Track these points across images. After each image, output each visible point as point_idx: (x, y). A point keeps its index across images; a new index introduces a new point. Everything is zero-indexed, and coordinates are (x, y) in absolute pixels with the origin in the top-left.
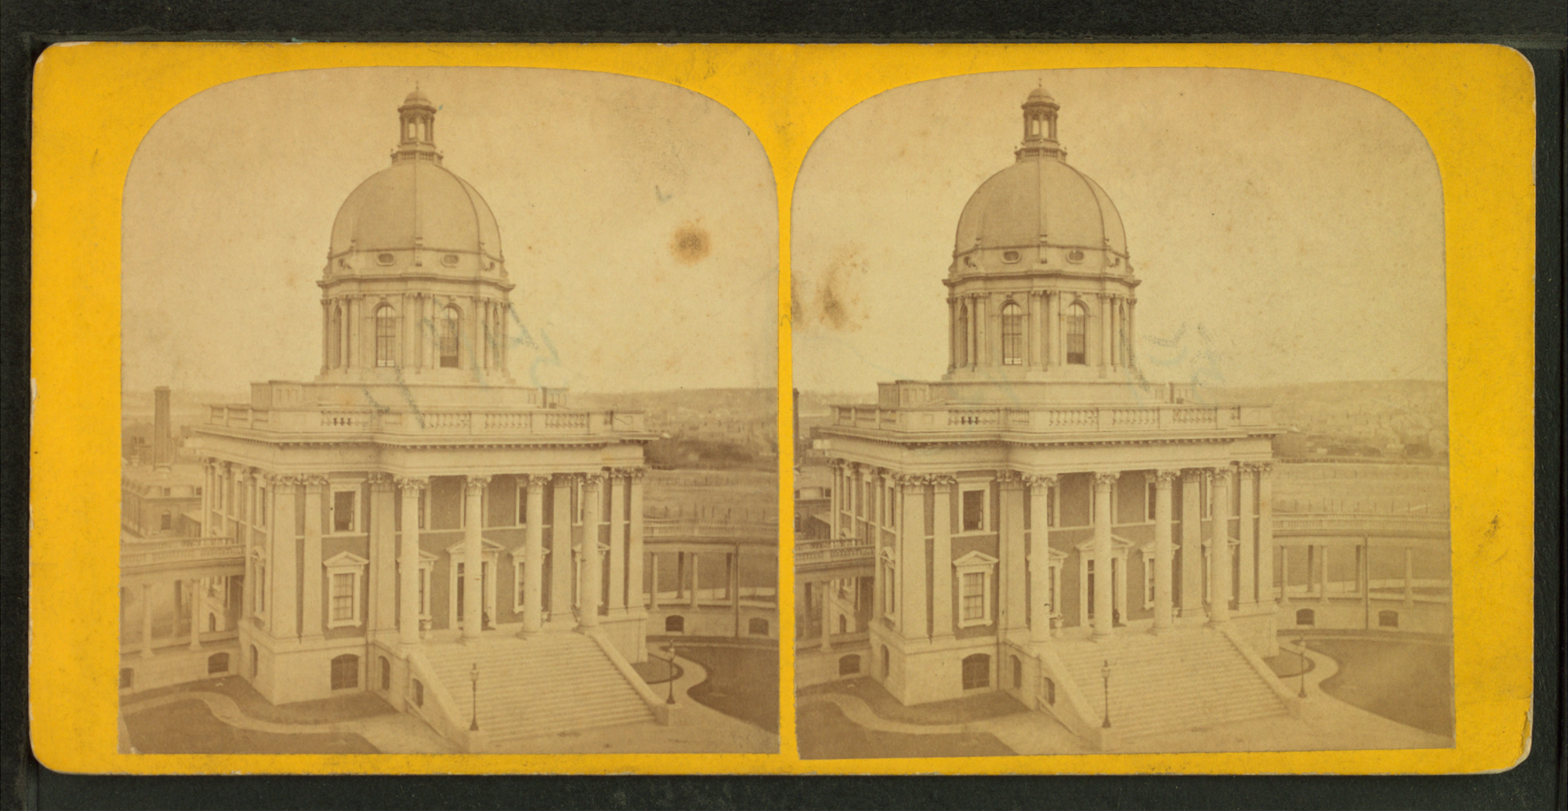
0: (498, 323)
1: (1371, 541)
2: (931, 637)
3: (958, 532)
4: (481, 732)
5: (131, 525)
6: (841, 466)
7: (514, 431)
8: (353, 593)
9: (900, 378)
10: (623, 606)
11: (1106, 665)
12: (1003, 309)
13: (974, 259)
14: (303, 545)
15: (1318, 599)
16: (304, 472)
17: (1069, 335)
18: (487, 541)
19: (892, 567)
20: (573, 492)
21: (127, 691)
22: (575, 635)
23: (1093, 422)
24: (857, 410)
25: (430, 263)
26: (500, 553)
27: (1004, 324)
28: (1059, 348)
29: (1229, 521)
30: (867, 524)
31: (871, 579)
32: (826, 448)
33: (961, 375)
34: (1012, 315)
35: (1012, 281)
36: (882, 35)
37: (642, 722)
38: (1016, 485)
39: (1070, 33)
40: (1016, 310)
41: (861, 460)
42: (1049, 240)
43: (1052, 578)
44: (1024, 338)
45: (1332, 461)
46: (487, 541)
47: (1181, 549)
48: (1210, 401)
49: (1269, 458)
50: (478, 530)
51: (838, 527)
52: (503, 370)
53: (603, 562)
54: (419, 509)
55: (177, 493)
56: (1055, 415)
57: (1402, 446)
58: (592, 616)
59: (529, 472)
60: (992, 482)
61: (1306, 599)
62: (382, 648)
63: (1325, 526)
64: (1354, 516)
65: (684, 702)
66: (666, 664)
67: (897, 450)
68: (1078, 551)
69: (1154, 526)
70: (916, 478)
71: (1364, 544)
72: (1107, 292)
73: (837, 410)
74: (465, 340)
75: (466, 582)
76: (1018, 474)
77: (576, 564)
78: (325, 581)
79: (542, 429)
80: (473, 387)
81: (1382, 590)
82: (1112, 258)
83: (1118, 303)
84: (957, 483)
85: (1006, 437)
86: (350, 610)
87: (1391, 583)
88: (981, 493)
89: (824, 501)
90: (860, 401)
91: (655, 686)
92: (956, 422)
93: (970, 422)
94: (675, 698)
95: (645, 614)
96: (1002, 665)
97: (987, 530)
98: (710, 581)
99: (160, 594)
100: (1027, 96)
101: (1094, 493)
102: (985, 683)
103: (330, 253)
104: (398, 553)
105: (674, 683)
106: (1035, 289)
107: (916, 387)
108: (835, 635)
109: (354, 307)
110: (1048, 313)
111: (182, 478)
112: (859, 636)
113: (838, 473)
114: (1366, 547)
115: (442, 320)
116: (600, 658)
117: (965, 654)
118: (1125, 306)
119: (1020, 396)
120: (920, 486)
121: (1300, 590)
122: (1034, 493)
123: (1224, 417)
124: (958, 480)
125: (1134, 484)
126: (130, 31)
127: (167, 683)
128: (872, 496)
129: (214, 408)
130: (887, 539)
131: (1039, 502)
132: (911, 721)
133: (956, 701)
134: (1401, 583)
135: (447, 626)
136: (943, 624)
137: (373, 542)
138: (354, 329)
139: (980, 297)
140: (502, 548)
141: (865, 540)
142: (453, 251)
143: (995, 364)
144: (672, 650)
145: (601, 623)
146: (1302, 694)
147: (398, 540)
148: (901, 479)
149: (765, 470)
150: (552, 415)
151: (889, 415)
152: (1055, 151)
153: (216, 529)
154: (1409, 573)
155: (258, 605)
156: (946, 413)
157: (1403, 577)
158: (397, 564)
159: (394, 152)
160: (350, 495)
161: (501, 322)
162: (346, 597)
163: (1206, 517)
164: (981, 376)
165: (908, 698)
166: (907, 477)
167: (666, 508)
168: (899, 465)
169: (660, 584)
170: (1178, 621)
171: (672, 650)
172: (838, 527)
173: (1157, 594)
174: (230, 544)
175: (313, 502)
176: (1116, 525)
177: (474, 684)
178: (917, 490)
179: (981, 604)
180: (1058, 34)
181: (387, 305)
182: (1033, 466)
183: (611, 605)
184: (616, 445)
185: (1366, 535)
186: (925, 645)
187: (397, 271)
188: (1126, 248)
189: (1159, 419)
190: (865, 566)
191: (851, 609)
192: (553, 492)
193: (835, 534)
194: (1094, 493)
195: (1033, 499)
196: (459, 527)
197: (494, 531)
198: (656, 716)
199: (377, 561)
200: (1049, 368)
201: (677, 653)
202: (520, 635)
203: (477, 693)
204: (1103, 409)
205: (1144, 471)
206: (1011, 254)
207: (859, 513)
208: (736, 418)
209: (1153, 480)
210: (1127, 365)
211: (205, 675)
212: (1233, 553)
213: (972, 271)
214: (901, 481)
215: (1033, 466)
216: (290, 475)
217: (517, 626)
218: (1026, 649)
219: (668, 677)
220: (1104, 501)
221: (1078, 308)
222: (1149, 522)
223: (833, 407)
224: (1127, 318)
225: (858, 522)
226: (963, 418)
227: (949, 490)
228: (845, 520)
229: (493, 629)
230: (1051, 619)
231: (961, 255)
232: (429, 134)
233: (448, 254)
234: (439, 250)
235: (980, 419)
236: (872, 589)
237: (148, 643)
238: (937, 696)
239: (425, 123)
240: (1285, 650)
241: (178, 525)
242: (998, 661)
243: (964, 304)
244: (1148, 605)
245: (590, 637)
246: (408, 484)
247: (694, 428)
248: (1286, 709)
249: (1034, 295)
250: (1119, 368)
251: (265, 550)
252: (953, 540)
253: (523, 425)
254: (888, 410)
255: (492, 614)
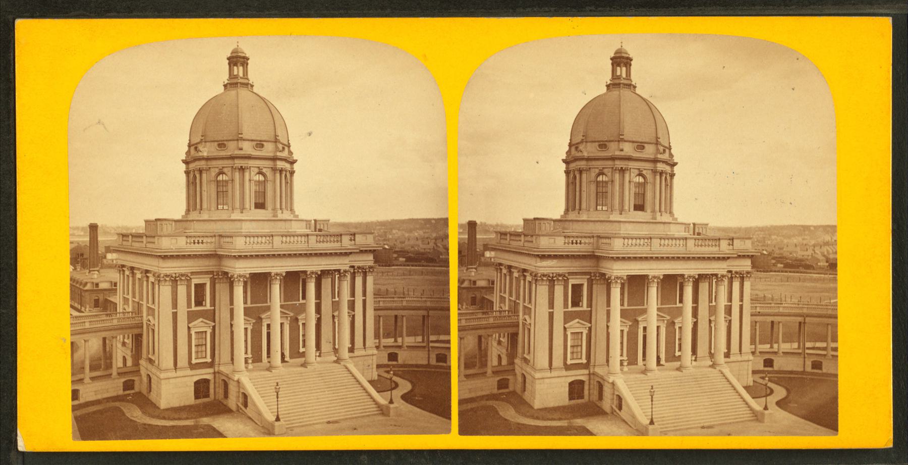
0: (287, 183)
1: (808, 319)
2: (551, 369)
3: (568, 308)
4: (282, 421)
5: (76, 305)
6: (501, 267)
7: (300, 245)
8: (582, 343)
9: (536, 217)
10: (363, 347)
11: (277, 385)
12: (597, 177)
13: (581, 147)
14: (553, 314)
15: (775, 353)
16: (176, 272)
17: (256, 192)
18: (283, 310)
19: (529, 327)
20: (710, 286)
21: (76, 402)
22: (710, 369)
23: (269, 242)
24: (511, 235)
25: (248, 148)
26: (291, 317)
27: (217, 186)
28: (250, 201)
29: (725, 305)
30: (515, 302)
31: (516, 334)
32: (493, 256)
33: (194, 215)
34: (223, 180)
35: (604, 161)
36: (511, 11)
37: (375, 415)
38: (225, 280)
39: (621, 8)
40: (225, 178)
41: (513, 264)
42: (244, 136)
43: (246, 335)
44: (609, 195)
45: (786, 272)
46: (283, 310)
47: (697, 321)
48: (717, 235)
49: (749, 269)
50: (279, 304)
51: (121, 305)
52: (291, 210)
53: (728, 327)
54: (621, 294)
55: (103, 286)
56: (248, 239)
57: (827, 264)
58: (345, 354)
59: (307, 270)
60: (588, 279)
61: (392, 346)
62: (598, 376)
63: (781, 310)
64: (798, 304)
65: (400, 405)
66: (389, 382)
67: (157, 260)
68: (261, 319)
69: (682, 307)
70: (544, 275)
71: (427, 314)
72: (278, 166)
73: (121, 236)
74: (269, 194)
75: (271, 334)
76: (226, 273)
77: (335, 323)
78: (565, 336)
79: (314, 244)
80: (653, 223)
81: (813, 348)
82: (280, 146)
83: (664, 176)
84: (568, 279)
85: (597, 252)
86: (580, 353)
87: (818, 345)
88: (582, 285)
89: (490, 287)
90: (134, 231)
91: (381, 393)
92: (190, 243)
93: (576, 243)
94: (394, 400)
95: (751, 357)
96: (217, 385)
97: (584, 307)
98: (788, 339)
99: (94, 345)
100: (230, 52)
101: (648, 287)
102: (207, 396)
103: (570, 143)
104: (608, 320)
105: (768, 398)
106: (235, 165)
107: (545, 222)
108: (495, 367)
109: (584, 176)
110: (623, 180)
111: (104, 278)
112: (135, 369)
113: (122, 272)
114: (805, 323)
115: (635, 183)
116: (350, 378)
117: (196, 379)
118: (668, 178)
119: (226, 228)
120: (169, 281)
121: (766, 347)
122: (613, 285)
123: (724, 245)
124: (569, 277)
125: (671, 283)
126: (71, 14)
127: (99, 397)
128: (141, 286)
129: (124, 236)
130: (150, 311)
131: (616, 292)
132: (537, 418)
133: (564, 407)
134: (824, 345)
135: (261, 361)
136: (183, 361)
137: (217, 312)
138: (584, 188)
139: (203, 170)
140: (292, 314)
141: (513, 311)
142: (261, 141)
143: (591, 210)
144: (767, 379)
145: (726, 363)
146: (766, 408)
147: (232, 311)
148: (535, 276)
149: (821, 274)
150: (698, 239)
151: (529, 238)
152: (247, 84)
153: (126, 307)
154: (829, 339)
155: (526, 351)
156: (563, 238)
157: (826, 341)
158: (232, 325)
159: (225, 83)
160: (580, 286)
161: (289, 182)
162: (577, 346)
163: (712, 303)
164: (205, 216)
165: (537, 405)
166: (162, 275)
167: (765, 296)
168: (157, 268)
169: (760, 341)
170: (318, 359)
171: (767, 379)
172: (121, 305)
173: (307, 344)
174: (510, 314)
175: (182, 290)
176: (660, 306)
177: (652, 398)
178: (167, 283)
179: (204, 350)
180: (614, 8)
181: (603, 174)
182: (235, 268)
183: (732, 352)
184: (736, 258)
185: (428, 309)
186: (172, 374)
187: (228, 153)
188: (288, 141)
189: (308, 241)
190: (138, 327)
191: (504, 351)
192: (321, 281)
193: (496, 307)
194: (648, 287)
195: (612, 289)
196: (644, 305)
197: (287, 305)
198: (383, 411)
199: (220, 323)
200: (623, 213)
201: (394, 374)
202: (679, 369)
203: (279, 399)
204: (722, 239)
205: (678, 275)
206: (603, 146)
207: (134, 296)
208: (805, 242)
209: (305, 277)
210: (289, 209)
211: (121, 392)
212: (727, 324)
213: (579, 154)
214: (158, 277)
215: (235, 268)
216: (168, 274)
217: (677, 364)
218: (605, 378)
219: (764, 394)
220: (653, 292)
221: (641, 177)
222: (678, 305)
223: (496, 232)
224: (289, 182)
225: (510, 300)
226: (572, 241)
227: (563, 283)
228: (502, 299)
229: (287, 362)
230: (621, 360)
231: (193, 145)
232: (246, 72)
233: (639, 144)
234: (252, 140)
235: (583, 241)
236: (517, 340)
237: (88, 374)
238: (552, 404)
239: (626, 67)
240: (756, 382)
241: (103, 304)
242: (215, 383)
243: (574, 174)
244: (677, 354)
245: (720, 371)
246: (540, 277)
247: (781, 249)
248: (757, 417)
249: (235, 169)
250: (285, 211)
251: (530, 318)
252: (565, 312)
253: (682, 245)
254: (528, 236)
255: (663, 356)
